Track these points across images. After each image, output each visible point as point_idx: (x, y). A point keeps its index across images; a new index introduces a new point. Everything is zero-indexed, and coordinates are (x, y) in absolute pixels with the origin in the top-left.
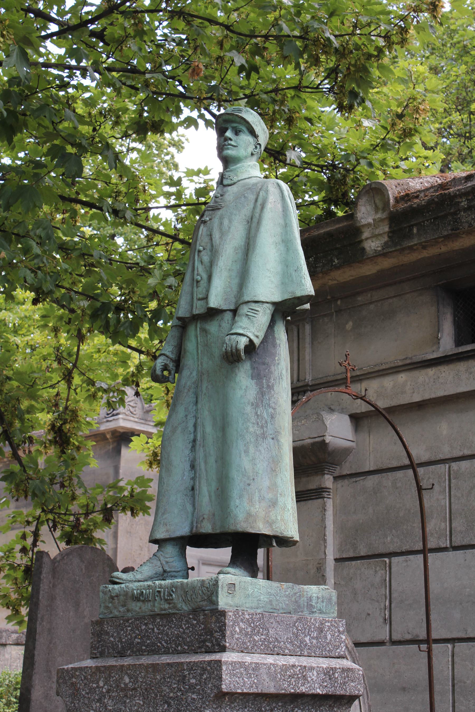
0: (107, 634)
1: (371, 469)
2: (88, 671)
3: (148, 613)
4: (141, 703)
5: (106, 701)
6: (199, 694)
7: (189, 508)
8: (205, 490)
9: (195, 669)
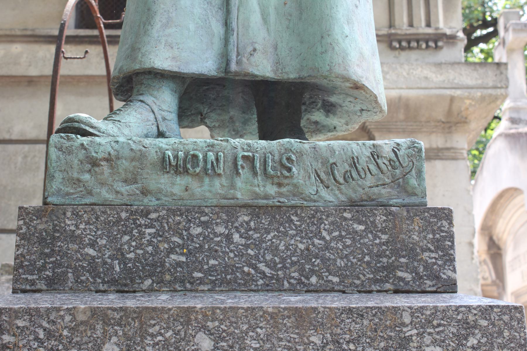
2: (62, 318)
3: (215, 202)
7: (218, 29)
9: (439, 325)
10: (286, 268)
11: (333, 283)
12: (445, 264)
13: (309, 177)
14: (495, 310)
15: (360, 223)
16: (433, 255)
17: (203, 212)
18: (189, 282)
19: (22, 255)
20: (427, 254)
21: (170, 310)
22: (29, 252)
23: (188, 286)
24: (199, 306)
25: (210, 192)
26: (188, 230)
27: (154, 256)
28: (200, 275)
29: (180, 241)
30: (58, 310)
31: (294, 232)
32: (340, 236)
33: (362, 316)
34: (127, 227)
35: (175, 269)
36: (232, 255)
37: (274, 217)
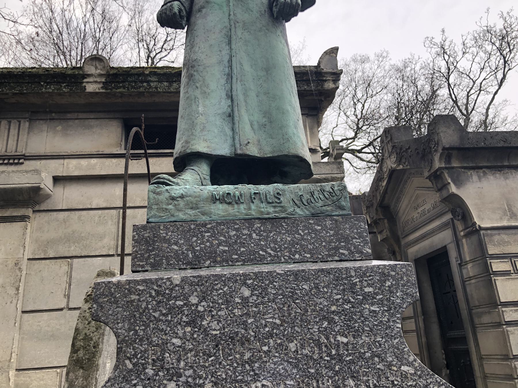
0: (168, 241)
1: (63, 208)
2: (165, 283)
3: (242, 217)
4: (278, 322)
5: (205, 323)
6: (383, 305)
7: (229, 132)
8: (245, 118)
10: (282, 251)
11: (307, 258)
12: (364, 245)
13: (290, 203)
14: (398, 266)
15: (318, 226)
16: (358, 241)
17: (236, 223)
18: (231, 261)
19: (136, 251)
20: (354, 240)
21: (225, 275)
22: (140, 250)
23: (230, 263)
24: (241, 272)
25: (238, 212)
26: (228, 233)
27: (210, 248)
28: (236, 257)
29: (224, 239)
30: (162, 279)
31: (285, 232)
32: (309, 232)
33: (329, 273)
34: (194, 233)
35: (222, 254)
36: (252, 245)
37: (273, 224)
